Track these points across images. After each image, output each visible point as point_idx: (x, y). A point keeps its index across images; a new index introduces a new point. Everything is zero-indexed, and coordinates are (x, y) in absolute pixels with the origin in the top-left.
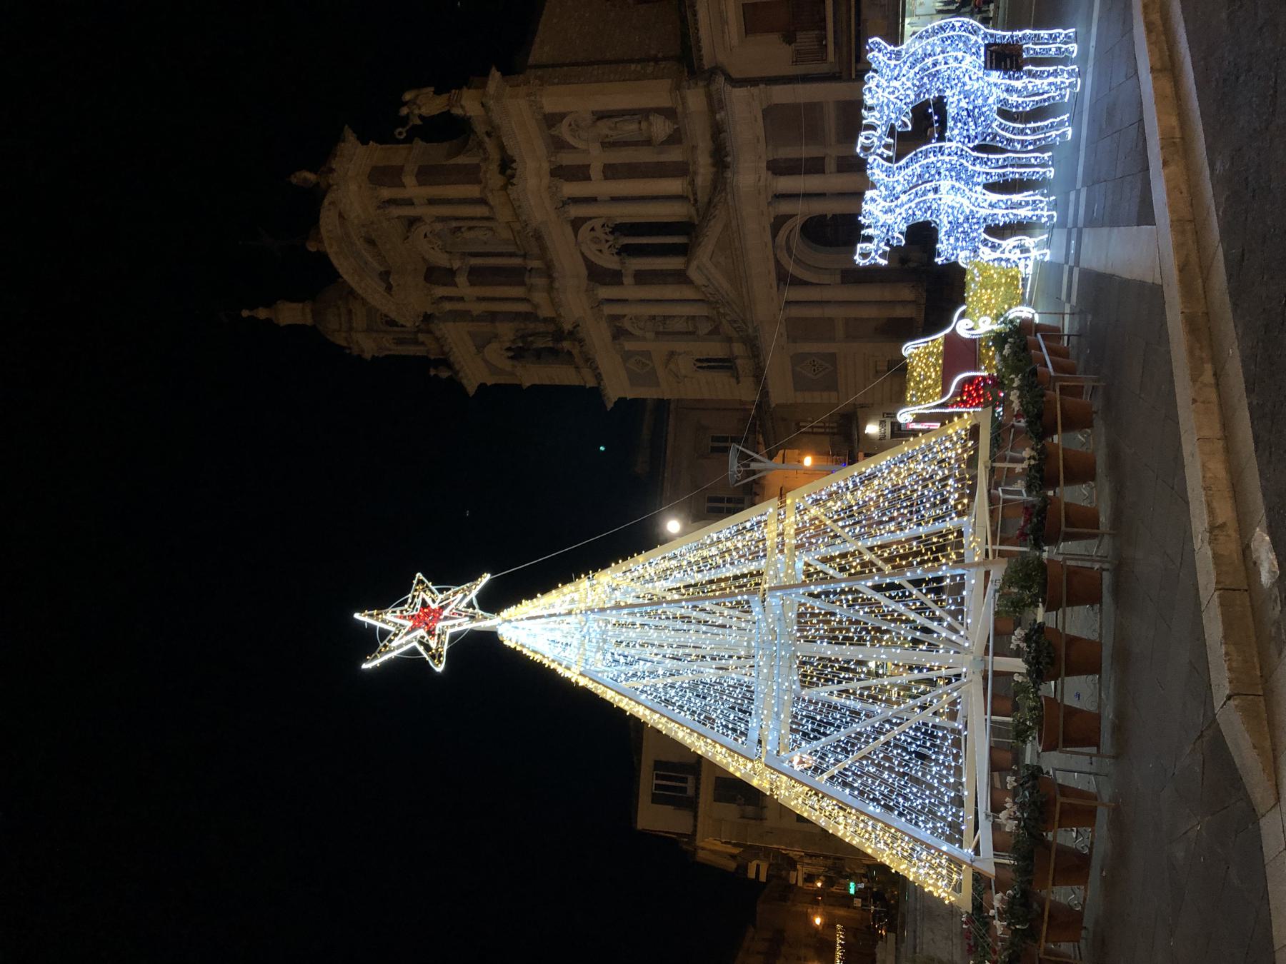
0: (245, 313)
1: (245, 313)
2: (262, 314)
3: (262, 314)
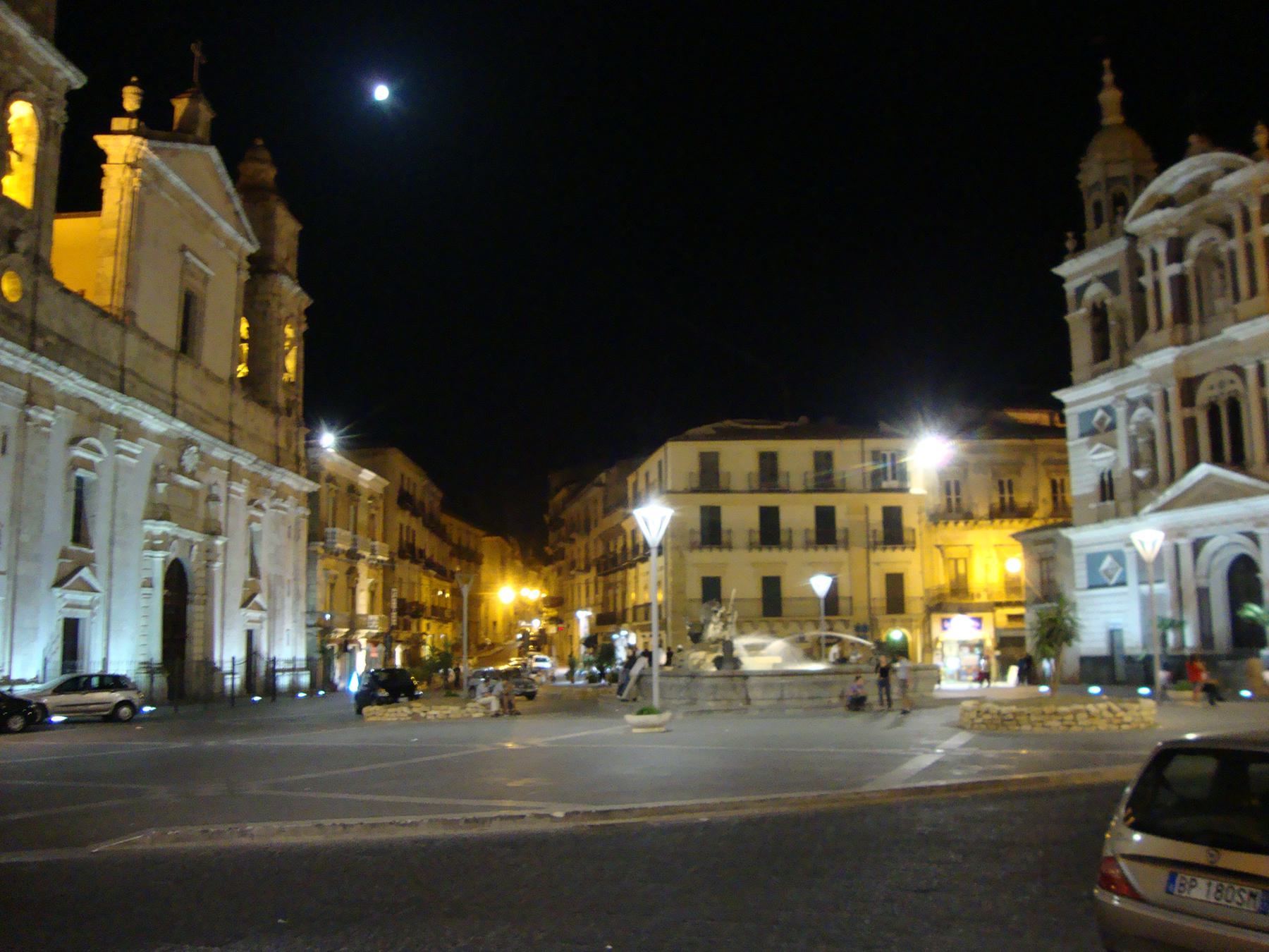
0: (1106, 63)
1: (1106, 63)
2: (1108, 78)
3: (1108, 78)
